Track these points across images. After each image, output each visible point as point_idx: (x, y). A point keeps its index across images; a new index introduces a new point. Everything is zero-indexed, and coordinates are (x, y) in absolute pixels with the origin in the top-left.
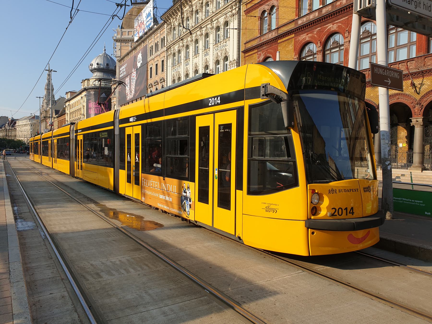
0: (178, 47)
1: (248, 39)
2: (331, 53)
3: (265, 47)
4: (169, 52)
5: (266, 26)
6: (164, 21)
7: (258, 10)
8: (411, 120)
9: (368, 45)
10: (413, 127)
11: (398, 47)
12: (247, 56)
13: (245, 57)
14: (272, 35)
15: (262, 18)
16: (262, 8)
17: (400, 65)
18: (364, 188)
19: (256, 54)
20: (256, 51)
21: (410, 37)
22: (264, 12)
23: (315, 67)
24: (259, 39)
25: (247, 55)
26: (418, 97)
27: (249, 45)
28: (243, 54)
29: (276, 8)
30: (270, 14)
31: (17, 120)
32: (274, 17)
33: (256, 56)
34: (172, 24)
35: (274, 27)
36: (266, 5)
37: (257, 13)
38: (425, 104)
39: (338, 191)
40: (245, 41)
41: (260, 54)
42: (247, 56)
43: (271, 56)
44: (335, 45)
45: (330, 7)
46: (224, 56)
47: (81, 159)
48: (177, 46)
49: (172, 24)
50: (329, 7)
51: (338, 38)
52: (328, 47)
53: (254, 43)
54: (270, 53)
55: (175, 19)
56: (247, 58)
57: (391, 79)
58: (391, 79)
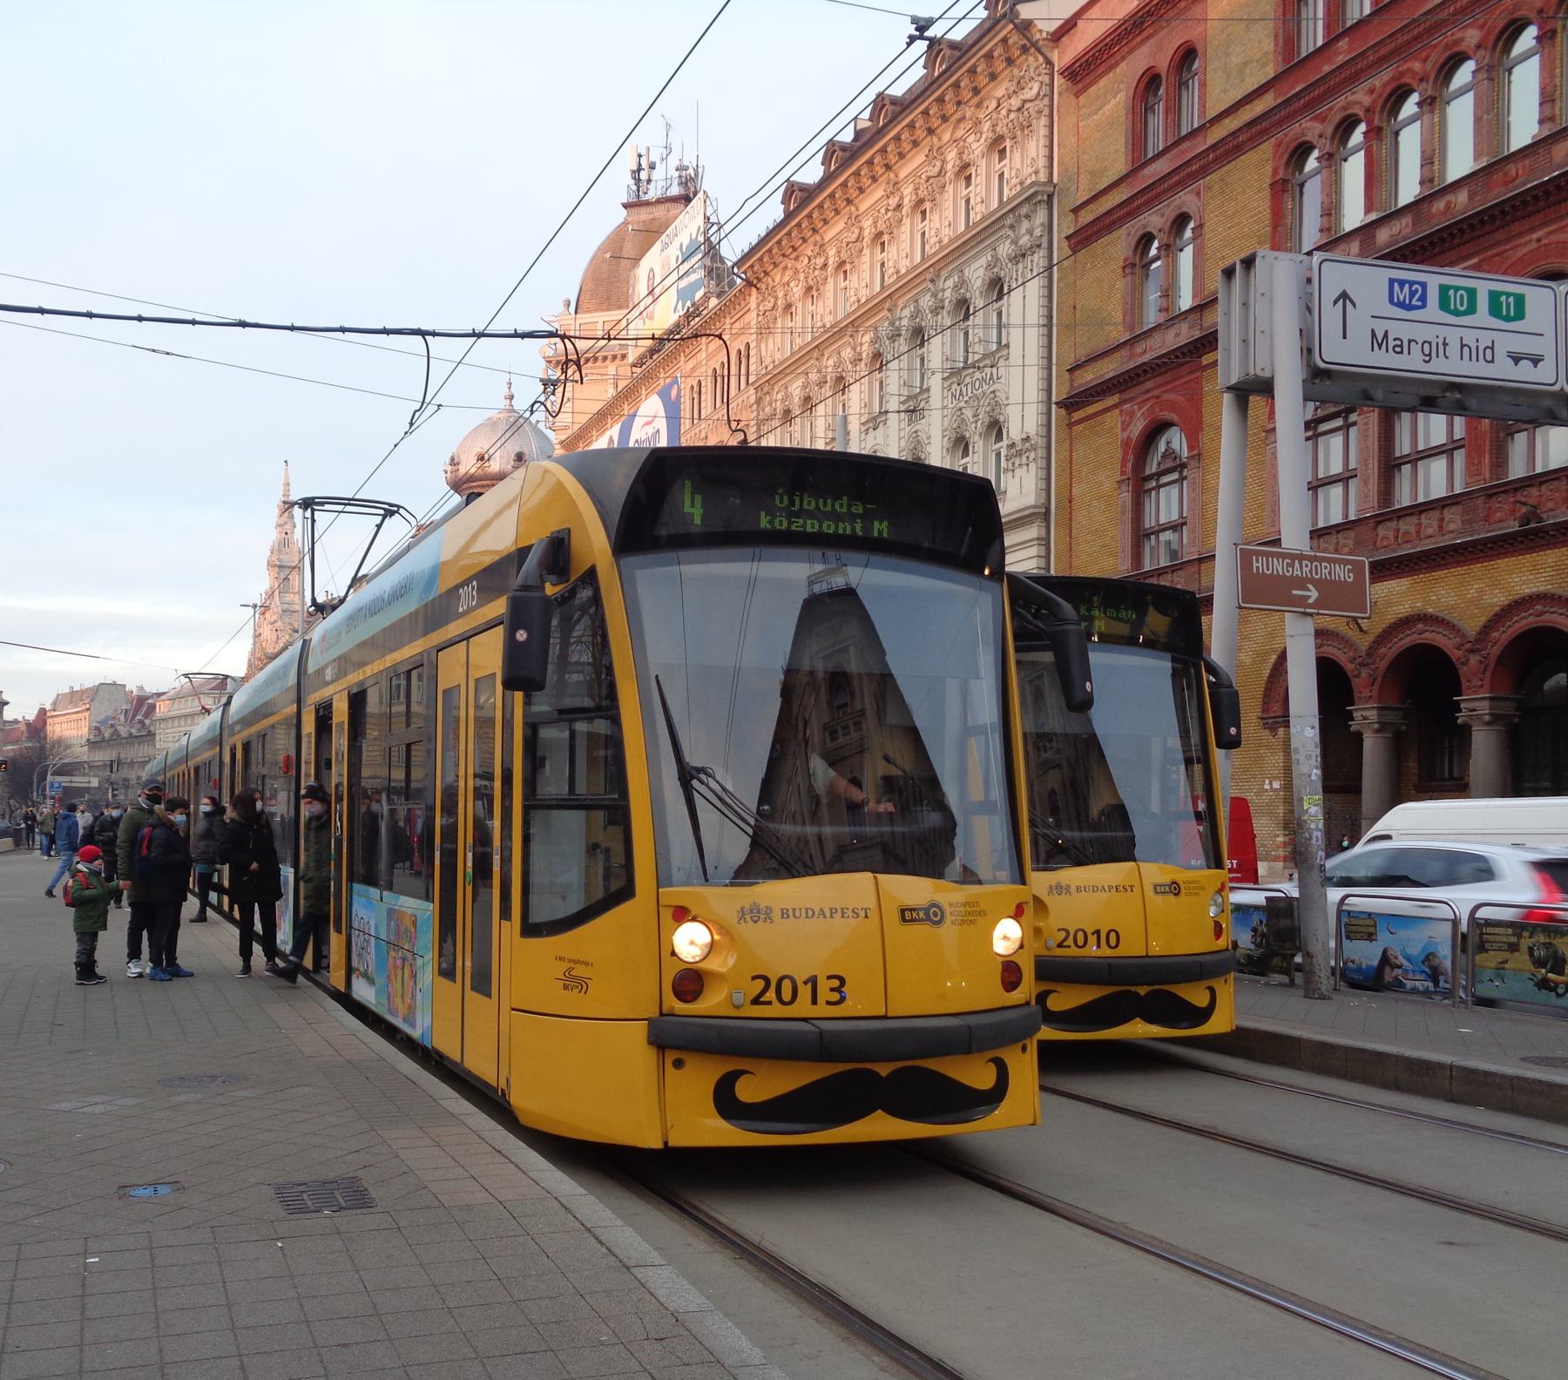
0: (804, 387)
1: (1083, 352)
2: (1159, 487)
3: (1149, 385)
4: (767, 409)
5: (1153, 297)
6: (746, 280)
7: (1123, 231)
8: (1350, 712)
9: (1174, 490)
10: (1359, 736)
11: (1420, 456)
12: (1079, 422)
13: (1070, 425)
14: (1177, 335)
15: (1138, 264)
16: (1134, 228)
17: (1544, 488)
18: (903, 911)
19: (1117, 411)
20: (1115, 399)
21: (1451, 426)
22: (1146, 239)
23: (987, 572)
24: (1125, 352)
25: (1077, 415)
26: (1364, 643)
27: (1089, 377)
28: (1063, 411)
29: (1192, 225)
30: (1166, 248)
31: (159, 695)
32: (1186, 258)
33: (1113, 419)
34: (781, 294)
35: (1186, 301)
36: (1315, 118)
37: (1119, 244)
38: (1495, 651)
39: (777, 914)
40: (1070, 361)
41: (1131, 414)
42: (1079, 422)
43: (1174, 417)
44: (1169, 464)
45: (1406, 221)
46: (987, 420)
47: (450, 833)
48: (799, 383)
49: (781, 294)
50: (1404, 221)
51: (1175, 440)
52: (1152, 467)
53: (1109, 369)
54: (1173, 407)
55: (789, 273)
56: (1080, 427)
57: (1318, 584)
58: (1318, 584)
